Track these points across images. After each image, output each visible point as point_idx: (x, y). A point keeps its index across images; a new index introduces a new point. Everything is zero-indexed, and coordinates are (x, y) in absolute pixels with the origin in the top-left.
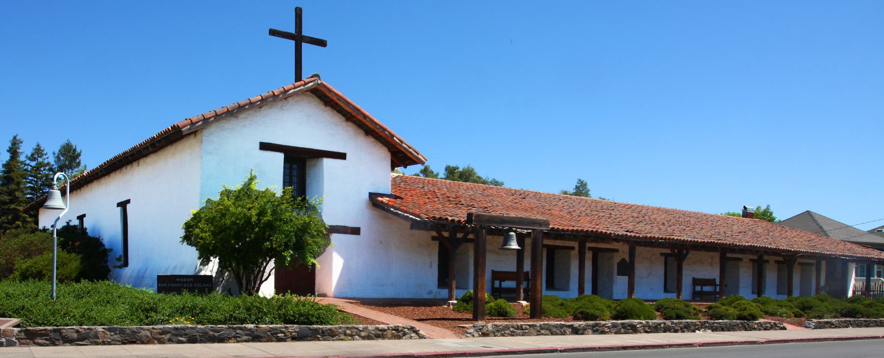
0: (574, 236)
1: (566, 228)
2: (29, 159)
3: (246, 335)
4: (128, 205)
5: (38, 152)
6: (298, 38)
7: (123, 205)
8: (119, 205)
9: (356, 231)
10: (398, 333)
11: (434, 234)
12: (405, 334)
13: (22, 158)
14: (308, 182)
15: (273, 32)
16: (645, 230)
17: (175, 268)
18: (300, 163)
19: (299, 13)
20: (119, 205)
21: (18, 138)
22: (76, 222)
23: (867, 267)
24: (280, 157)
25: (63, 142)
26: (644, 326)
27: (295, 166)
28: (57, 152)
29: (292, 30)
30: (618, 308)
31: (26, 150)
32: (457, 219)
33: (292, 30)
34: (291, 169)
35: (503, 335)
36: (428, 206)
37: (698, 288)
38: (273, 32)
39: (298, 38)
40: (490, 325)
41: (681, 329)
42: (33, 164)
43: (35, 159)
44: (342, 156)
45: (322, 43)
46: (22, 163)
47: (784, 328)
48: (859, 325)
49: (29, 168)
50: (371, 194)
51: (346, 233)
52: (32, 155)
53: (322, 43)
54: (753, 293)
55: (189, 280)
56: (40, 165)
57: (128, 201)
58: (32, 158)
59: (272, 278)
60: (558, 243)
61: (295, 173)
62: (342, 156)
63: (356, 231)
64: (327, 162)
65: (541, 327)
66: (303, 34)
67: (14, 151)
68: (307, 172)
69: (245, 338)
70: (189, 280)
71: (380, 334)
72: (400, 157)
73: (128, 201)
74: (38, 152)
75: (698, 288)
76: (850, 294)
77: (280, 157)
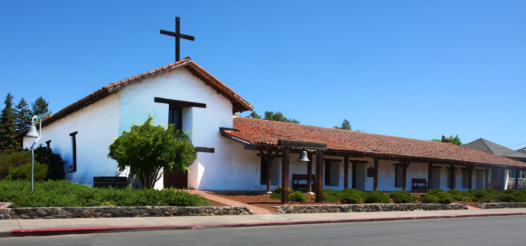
1: (337, 149)
2: (17, 107)
3: (146, 212)
4: (76, 135)
5: (23, 103)
6: (178, 35)
7: (73, 135)
8: (71, 135)
9: (212, 150)
10: (237, 211)
11: (258, 152)
12: (241, 212)
13: (13, 107)
15: (162, 32)
16: (384, 150)
17: (104, 172)
18: (178, 110)
19: (178, 20)
20: (71, 135)
21: (11, 95)
22: (45, 145)
23: (516, 172)
25: (38, 97)
27: (175, 112)
28: (34, 103)
29: (174, 30)
31: (15, 102)
32: (272, 143)
33: (174, 30)
34: (173, 113)
37: (415, 185)
38: (162, 32)
39: (178, 35)
41: (405, 209)
42: (20, 110)
43: (21, 108)
44: (203, 106)
45: (191, 38)
46: (13, 110)
48: (511, 207)
49: (18, 113)
50: (221, 128)
52: (19, 105)
53: (191, 38)
54: (448, 187)
55: (112, 179)
56: (24, 111)
57: (76, 133)
58: (19, 107)
59: (162, 179)
60: (332, 157)
61: (175, 116)
62: (203, 106)
63: (212, 150)
64: (194, 109)
65: (322, 208)
66: (181, 33)
67: (8, 103)
68: (183, 115)
69: (146, 214)
70: (112, 179)
71: (226, 212)
72: (238, 106)
73: (76, 133)
74: (23, 103)
75: (415, 185)
76: (506, 188)
77: (167, 106)
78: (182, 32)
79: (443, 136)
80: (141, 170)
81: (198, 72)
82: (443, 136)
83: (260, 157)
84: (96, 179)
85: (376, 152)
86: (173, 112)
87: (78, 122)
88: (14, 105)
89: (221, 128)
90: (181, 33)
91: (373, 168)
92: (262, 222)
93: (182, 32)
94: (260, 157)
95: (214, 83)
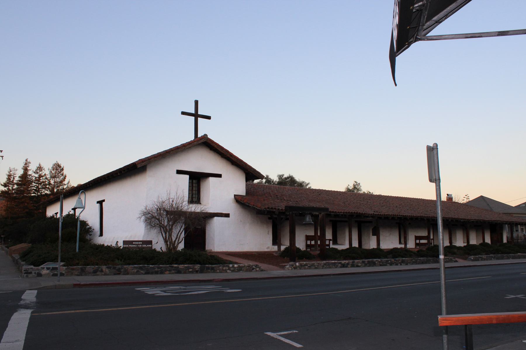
0: (345, 215)
1: (340, 211)
2: (34, 172)
3: (174, 270)
4: (103, 203)
5: (40, 168)
6: (196, 116)
7: (101, 203)
8: (98, 202)
9: (227, 215)
10: (250, 269)
11: (269, 216)
12: (253, 269)
13: (30, 173)
14: (201, 190)
15: (183, 113)
16: (384, 211)
17: (131, 237)
18: (197, 179)
19: (196, 102)
20: (98, 202)
21: (28, 161)
22: (72, 212)
23: (513, 225)
24: (187, 177)
25: (55, 162)
26: (380, 262)
27: (194, 181)
28: (51, 168)
29: (193, 111)
30: (227, 268)
31: (32, 168)
32: (281, 208)
33: (193, 111)
34: (192, 183)
35: (305, 269)
36: (266, 202)
37: (418, 241)
38: (183, 113)
39: (196, 116)
40: (297, 264)
41: (400, 263)
42: (37, 176)
43: (37, 173)
44: (219, 176)
45: (209, 118)
46: (30, 175)
47: (456, 261)
48: (498, 259)
49: (34, 178)
50: (235, 195)
51: (222, 217)
52: (36, 170)
53: (209, 118)
54: (464, 243)
55: (140, 243)
56: (40, 176)
57: (104, 201)
58: (36, 172)
59: (183, 241)
60: (338, 219)
61: (194, 185)
62: (219, 176)
63: (227, 215)
64: (211, 179)
65: (325, 264)
66: (199, 113)
67: (26, 169)
68: (201, 184)
69: (173, 272)
70: (140, 243)
71: (240, 269)
72: (250, 174)
73: (104, 201)
74: (40, 168)
75: (418, 241)
76: (505, 241)
77: (187, 177)
78: (200, 113)
79: (448, 195)
80: (13, 181)
81: (214, 147)
82: (448, 195)
83: (271, 220)
84: (124, 241)
85: (377, 213)
86: (192, 181)
87: (110, 194)
88: (31, 171)
89: (235, 195)
90: (199, 113)
91: (22, 302)
92: (272, 276)
93: (200, 113)
94: (271, 220)
95: (229, 156)
